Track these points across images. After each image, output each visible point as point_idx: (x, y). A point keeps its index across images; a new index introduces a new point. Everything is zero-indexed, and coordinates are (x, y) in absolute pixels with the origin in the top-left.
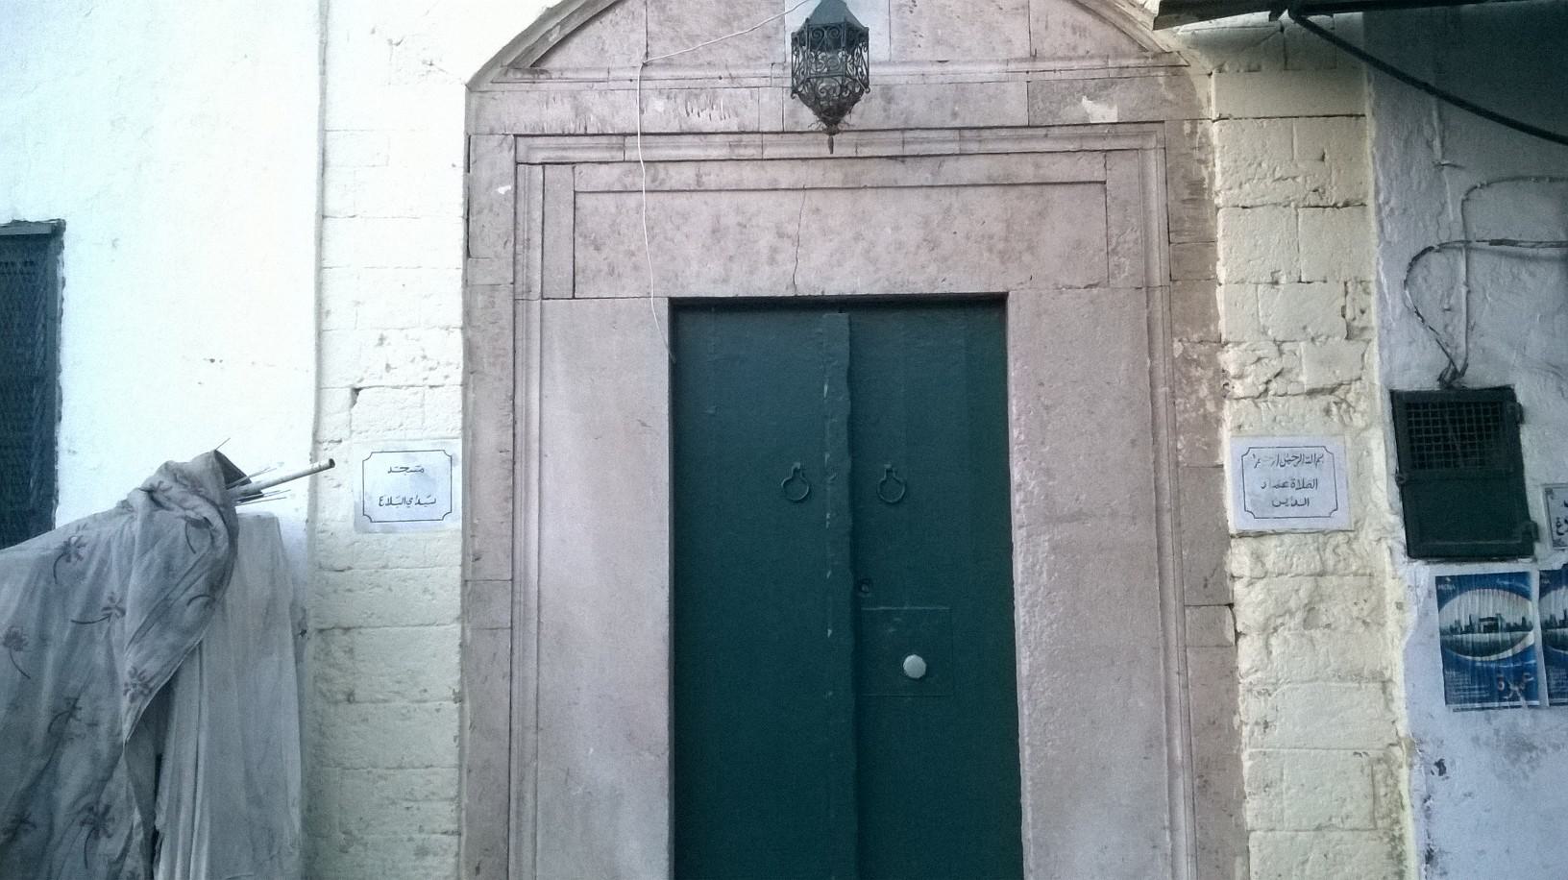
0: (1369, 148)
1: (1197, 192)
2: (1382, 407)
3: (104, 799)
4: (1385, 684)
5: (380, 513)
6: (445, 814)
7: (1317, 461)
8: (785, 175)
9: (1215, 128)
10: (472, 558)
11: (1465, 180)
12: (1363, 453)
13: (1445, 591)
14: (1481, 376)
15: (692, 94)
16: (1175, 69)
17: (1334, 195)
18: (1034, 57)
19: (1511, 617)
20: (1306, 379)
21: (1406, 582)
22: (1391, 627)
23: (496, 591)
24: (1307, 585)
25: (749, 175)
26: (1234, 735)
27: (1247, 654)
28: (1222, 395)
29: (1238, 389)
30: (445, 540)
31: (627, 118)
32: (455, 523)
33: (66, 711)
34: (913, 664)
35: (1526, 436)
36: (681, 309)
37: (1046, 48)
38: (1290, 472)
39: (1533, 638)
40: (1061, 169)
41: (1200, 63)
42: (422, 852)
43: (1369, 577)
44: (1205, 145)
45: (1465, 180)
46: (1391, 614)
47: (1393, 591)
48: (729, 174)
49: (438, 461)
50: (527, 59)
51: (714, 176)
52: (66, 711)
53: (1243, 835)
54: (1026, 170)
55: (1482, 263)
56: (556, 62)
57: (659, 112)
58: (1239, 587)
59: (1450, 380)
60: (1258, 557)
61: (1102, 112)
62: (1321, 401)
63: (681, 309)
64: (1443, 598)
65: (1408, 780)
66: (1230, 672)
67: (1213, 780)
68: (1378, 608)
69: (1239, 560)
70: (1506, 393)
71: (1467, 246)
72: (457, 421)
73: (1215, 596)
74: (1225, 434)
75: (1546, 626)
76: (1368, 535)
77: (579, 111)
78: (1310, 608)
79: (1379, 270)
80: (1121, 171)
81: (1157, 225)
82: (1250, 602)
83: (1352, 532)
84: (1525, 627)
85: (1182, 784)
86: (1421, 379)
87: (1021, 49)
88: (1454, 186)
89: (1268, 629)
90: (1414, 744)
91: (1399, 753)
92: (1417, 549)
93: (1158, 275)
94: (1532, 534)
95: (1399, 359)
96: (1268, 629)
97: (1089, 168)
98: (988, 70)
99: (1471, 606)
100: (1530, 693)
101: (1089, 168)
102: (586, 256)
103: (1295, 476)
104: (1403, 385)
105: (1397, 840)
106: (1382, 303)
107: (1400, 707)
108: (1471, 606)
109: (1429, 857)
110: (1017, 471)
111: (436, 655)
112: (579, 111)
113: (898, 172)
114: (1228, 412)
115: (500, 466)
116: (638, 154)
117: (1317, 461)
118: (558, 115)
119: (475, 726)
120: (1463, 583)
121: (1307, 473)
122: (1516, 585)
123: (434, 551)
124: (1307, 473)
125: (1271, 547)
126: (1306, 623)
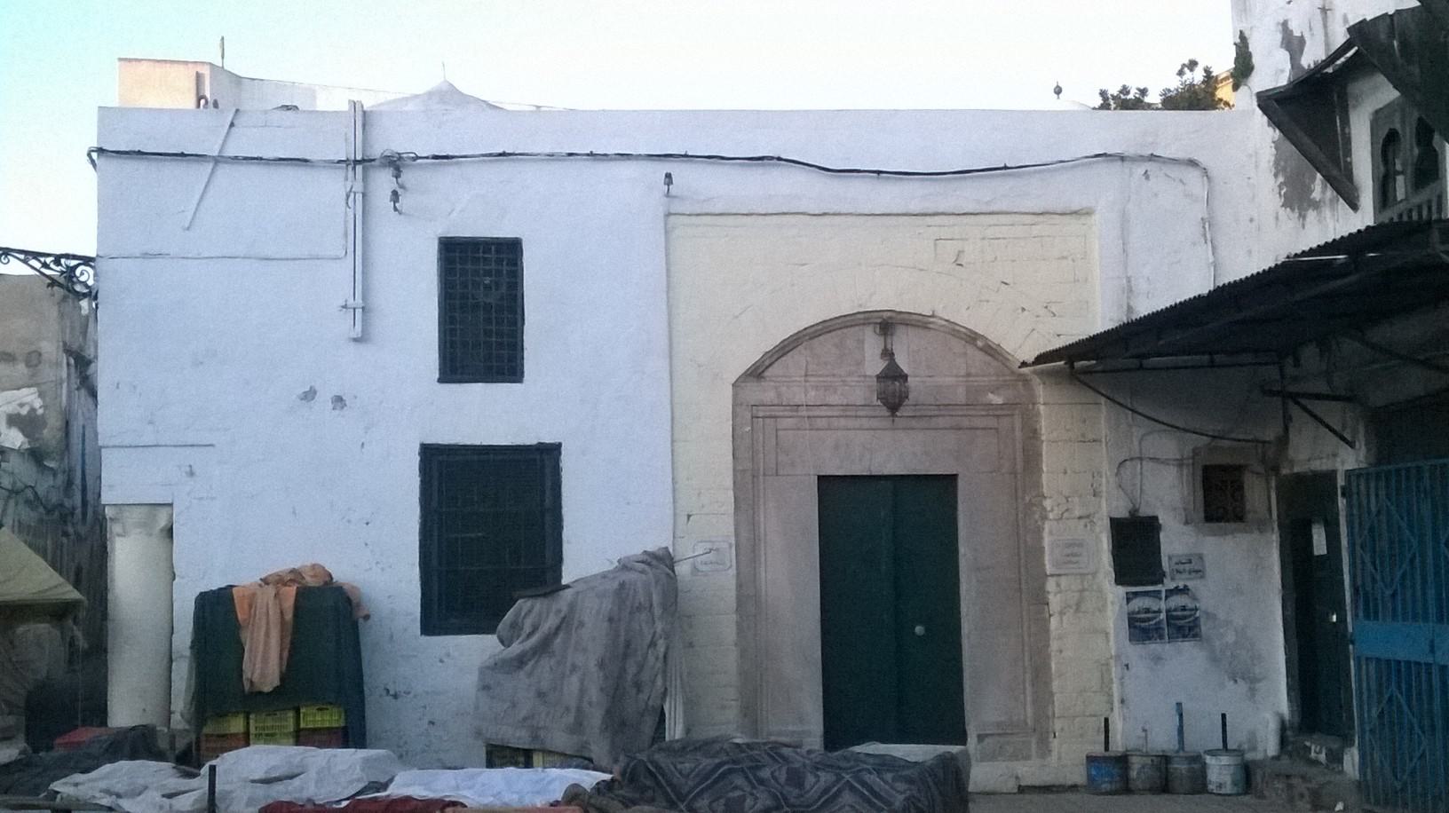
0: (1103, 418)
1: (1033, 434)
2: (1107, 522)
3: (632, 670)
4: (1107, 634)
5: (704, 568)
6: (732, 693)
7: (1080, 545)
8: (866, 423)
9: (1042, 408)
10: (739, 586)
11: (1142, 431)
12: (1098, 540)
13: (1130, 597)
14: (1145, 511)
15: (826, 389)
16: (1026, 381)
17: (1090, 436)
18: (968, 375)
19: (1190, 606)
20: (1077, 513)
21: (1115, 594)
22: (1109, 613)
23: (749, 599)
24: (1077, 595)
25: (851, 423)
26: (1049, 656)
27: (1054, 622)
28: (1044, 518)
29: (1051, 516)
30: (728, 580)
31: (799, 398)
32: (733, 572)
33: (628, 644)
34: (919, 630)
35: (1162, 535)
36: (823, 480)
37: (973, 371)
38: (1069, 551)
39: (1163, 616)
40: (978, 422)
41: (1036, 380)
42: (723, 707)
43: (1100, 591)
44: (1038, 414)
45: (1142, 431)
46: (1110, 607)
47: (1110, 597)
48: (843, 422)
49: (725, 545)
50: (756, 373)
51: (835, 423)
52: (628, 644)
53: (1052, 694)
54: (966, 422)
55: (1148, 465)
56: (767, 374)
57: (813, 396)
58: (1051, 597)
59: (1134, 512)
60: (1058, 585)
61: (997, 399)
62: (1082, 522)
63: (823, 480)
64: (1128, 600)
65: (1115, 672)
66: (1047, 631)
67: (1040, 673)
68: (1104, 605)
69: (1051, 585)
70: (1155, 518)
71: (1141, 459)
72: (732, 529)
73: (1041, 600)
74: (1046, 534)
75: (1168, 611)
76: (1101, 576)
77: (779, 395)
78: (1078, 605)
79: (1107, 469)
80: (1005, 422)
81: (1019, 446)
82: (1055, 601)
83: (1094, 574)
84: (1159, 611)
85: (1028, 676)
86: (1122, 513)
87: (963, 372)
88: (1137, 433)
89: (1062, 613)
90: (1118, 657)
91: (1112, 662)
92: (1120, 580)
93: (1019, 467)
94: (1164, 575)
95: (1113, 505)
96: (1062, 613)
97: (992, 422)
98: (949, 380)
99: (1138, 603)
100: (1161, 637)
101: (992, 422)
102: (782, 458)
103: (1073, 550)
104: (1116, 515)
105: (1110, 696)
106: (1107, 482)
107: (1112, 643)
108: (1138, 603)
109: (1122, 701)
110: (962, 549)
111: (728, 628)
112: (779, 395)
113: (914, 423)
114: (1047, 526)
115: (749, 547)
116: (805, 413)
117: (1080, 545)
118: (770, 396)
119: (743, 654)
120: (1136, 594)
121: (1076, 550)
122: (1156, 594)
123: (726, 582)
124: (1076, 550)
125: (1063, 580)
126: (1077, 610)
